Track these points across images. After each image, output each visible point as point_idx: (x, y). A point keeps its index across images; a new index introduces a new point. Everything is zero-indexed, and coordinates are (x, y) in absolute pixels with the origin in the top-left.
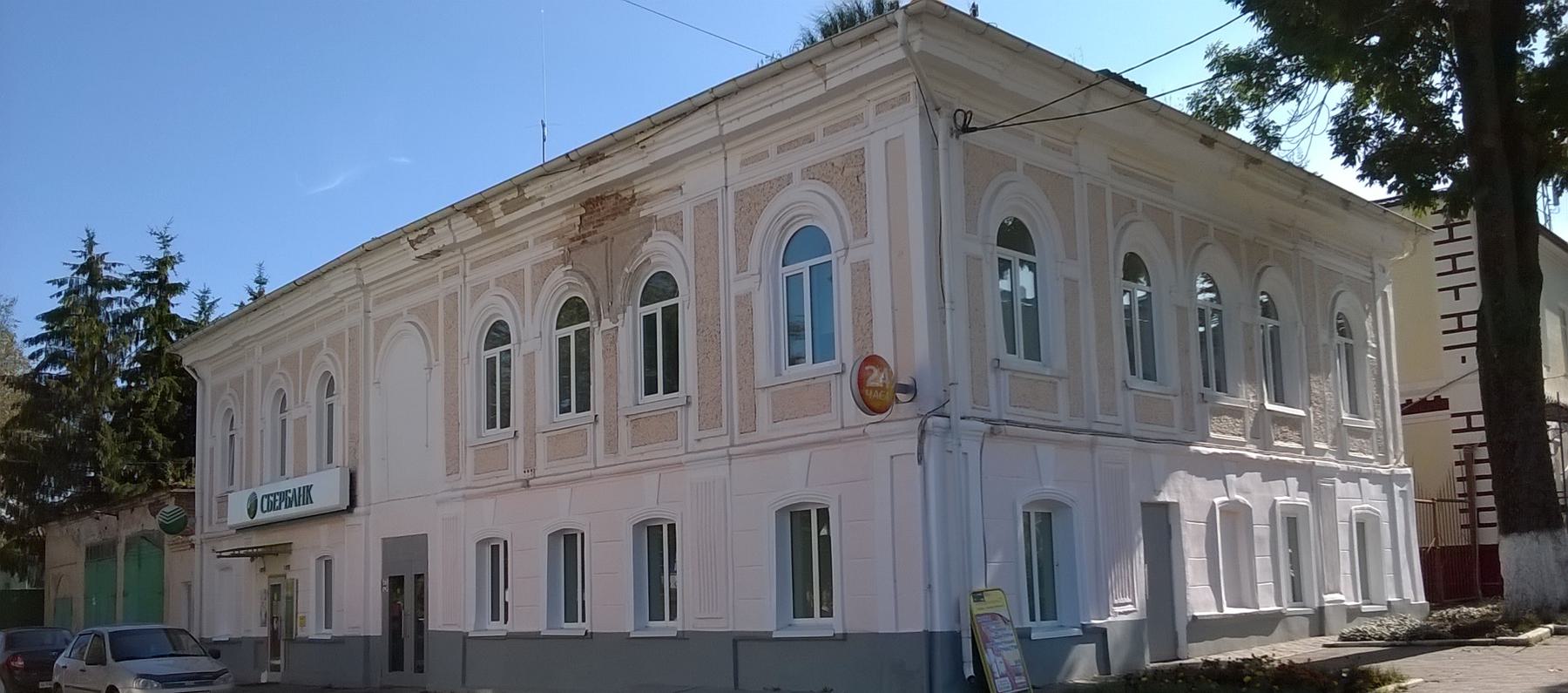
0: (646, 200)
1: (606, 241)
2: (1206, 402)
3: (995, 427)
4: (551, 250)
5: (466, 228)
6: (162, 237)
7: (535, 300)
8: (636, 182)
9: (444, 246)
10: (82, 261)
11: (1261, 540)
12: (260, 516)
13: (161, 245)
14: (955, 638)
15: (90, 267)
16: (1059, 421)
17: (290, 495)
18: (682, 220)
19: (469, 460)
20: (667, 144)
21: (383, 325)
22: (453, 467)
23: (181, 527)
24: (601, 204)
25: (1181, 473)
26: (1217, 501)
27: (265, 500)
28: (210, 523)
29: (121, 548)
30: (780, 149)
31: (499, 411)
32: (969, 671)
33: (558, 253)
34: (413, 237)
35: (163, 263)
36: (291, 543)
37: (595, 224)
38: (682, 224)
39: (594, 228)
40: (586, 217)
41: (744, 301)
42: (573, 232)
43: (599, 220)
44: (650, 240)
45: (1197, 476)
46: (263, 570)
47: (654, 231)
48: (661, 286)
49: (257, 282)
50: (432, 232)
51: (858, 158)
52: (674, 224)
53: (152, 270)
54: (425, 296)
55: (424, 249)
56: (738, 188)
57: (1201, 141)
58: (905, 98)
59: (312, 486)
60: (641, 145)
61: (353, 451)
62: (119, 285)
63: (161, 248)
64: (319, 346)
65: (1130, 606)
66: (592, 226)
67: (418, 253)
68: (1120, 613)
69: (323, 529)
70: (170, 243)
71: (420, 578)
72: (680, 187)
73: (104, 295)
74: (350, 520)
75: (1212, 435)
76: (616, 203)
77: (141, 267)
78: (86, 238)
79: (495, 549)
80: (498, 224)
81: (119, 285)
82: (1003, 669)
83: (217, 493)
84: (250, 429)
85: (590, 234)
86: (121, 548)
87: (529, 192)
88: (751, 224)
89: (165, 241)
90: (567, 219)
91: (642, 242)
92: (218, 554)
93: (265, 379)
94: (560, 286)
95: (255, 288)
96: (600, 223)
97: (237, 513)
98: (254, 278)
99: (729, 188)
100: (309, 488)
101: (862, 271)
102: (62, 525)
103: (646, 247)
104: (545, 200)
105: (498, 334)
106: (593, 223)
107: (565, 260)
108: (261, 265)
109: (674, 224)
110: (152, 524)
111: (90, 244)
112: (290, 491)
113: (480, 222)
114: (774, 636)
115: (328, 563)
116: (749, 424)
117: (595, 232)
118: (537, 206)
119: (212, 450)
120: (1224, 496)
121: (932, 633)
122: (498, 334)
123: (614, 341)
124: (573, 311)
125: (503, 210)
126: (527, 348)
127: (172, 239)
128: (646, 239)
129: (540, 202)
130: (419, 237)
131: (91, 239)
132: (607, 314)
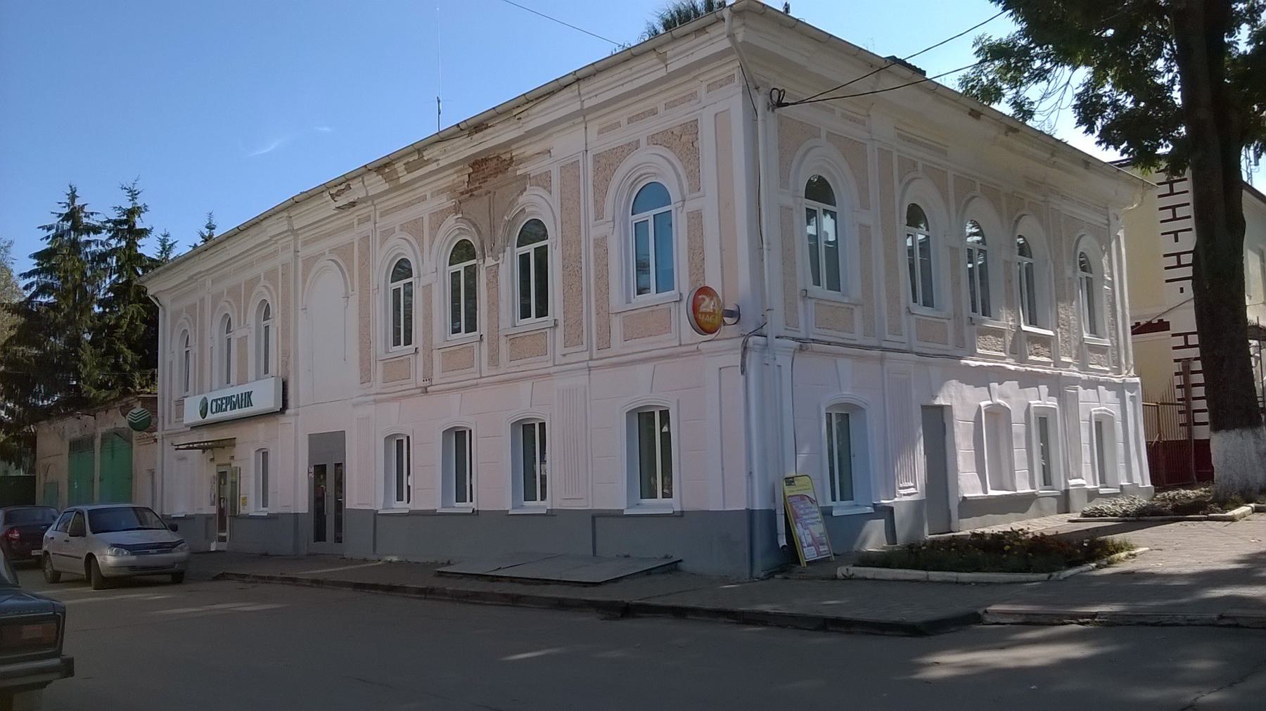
0: (521, 162)
1: (489, 195)
2: (974, 324)
3: (803, 344)
4: (445, 202)
5: (377, 184)
6: (131, 191)
7: (432, 242)
8: (513, 147)
9: (358, 198)
10: (66, 210)
11: (1018, 436)
12: (210, 417)
13: (130, 198)
14: (771, 514)
15: (73, 215)
16: (855, 340)
17: (234, 399)
18: (550, 177)
19: (378, 371)
20: (538, 117)
21: (309, 262)
22: (366, 376)
23: (146, 426)
24: (486, 165)
25: (954, 382)
26: (983, 404)
27: (214, 404)
28: (170, 422)
29: (98, 442)
30: (630, 121)
31: (403, 332)
32: (783, 542)
33: (451, 204)
34: (333, 191)
35: (132, 213)
36: (235, 438)
37: (481, 181)
38: (550, 181)
39: (479, 184)
40: (473, 175)
41: (601, 243)
42: (463, 187)
43: (484, 178)
44: (525, 194)
45: (967, 384)
46: (212, 460)
47: (528, 186)
48: (534, 231)
49: (207, 227)
50: (349, 187)
51: (692, 127)
52: (544, 181)
53: (122, 218)
54: (344, 238)
55: (342, 201)
56: (596, 151)
57: (970, 114)
58: (730, 79)
59: (252, 392)
60: (517, 117)
61: (285, 364)
62: (97, 230)
63: (130, 200)
64: (257, 279)
65: (912, 489)
66: (478, 182)
67: (340, 204)
68: (904, 495)
69: (261, 427)
70: (137, 196)
71: (339, 466)
72: (549, 151)
73: (84, 238)
74: (282, 419)
75: (979, 351)
76: (498, 164)
77: (114, 216)
78: (69, 192)
79: (400, 443)
80: (402, 181)
81: (97, 230)
82: (810, 540)
83: (176, 397)
84: (201, 346)
85: (476, 189)
86: (98, 442)
87: (427, 155)
88: (607, 181)
89: (133, 195)
90: (458, 177)
91: (518, 195)
92: (177, 447)
93: (214, 307)
94: (452, 230)
95: (206, 233)
96: (485, 180)
97: (192, 414)
98: (205, 224)
99: (588, 152)
100: (249, 394)
101: (696, 219)
102: (50, 424)
103: (521, 199)
104: (440, 162)
105: (402, 270)
106: (479, 180)
107: (456, 210)
108: (210, 214)
109: (544, 181)
110: (123, 423)
111: (73, 197)
112: (234, 396)
113: (388, 179)
114: (625, 513)
115: (265, 455)
116: (605, 343)
117: (480, 187)
118: (433, 167)
119: (171, 363)
120: (988, 400)
121: (753, 511)
122: (402, 270)
123: (496, 275)
124: (463, 251)
125: (406, 169)
126: (425, 280)
127: (139, 193)
128: (522, 193)
129: (435, 164)
130: (338, 191)
131: (73, 193)
132: (490, 253)
